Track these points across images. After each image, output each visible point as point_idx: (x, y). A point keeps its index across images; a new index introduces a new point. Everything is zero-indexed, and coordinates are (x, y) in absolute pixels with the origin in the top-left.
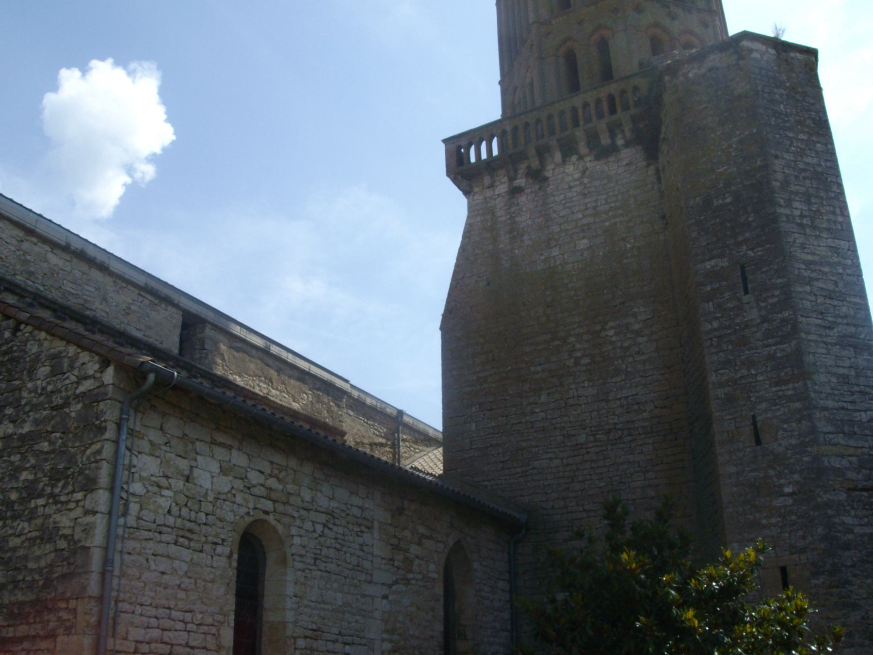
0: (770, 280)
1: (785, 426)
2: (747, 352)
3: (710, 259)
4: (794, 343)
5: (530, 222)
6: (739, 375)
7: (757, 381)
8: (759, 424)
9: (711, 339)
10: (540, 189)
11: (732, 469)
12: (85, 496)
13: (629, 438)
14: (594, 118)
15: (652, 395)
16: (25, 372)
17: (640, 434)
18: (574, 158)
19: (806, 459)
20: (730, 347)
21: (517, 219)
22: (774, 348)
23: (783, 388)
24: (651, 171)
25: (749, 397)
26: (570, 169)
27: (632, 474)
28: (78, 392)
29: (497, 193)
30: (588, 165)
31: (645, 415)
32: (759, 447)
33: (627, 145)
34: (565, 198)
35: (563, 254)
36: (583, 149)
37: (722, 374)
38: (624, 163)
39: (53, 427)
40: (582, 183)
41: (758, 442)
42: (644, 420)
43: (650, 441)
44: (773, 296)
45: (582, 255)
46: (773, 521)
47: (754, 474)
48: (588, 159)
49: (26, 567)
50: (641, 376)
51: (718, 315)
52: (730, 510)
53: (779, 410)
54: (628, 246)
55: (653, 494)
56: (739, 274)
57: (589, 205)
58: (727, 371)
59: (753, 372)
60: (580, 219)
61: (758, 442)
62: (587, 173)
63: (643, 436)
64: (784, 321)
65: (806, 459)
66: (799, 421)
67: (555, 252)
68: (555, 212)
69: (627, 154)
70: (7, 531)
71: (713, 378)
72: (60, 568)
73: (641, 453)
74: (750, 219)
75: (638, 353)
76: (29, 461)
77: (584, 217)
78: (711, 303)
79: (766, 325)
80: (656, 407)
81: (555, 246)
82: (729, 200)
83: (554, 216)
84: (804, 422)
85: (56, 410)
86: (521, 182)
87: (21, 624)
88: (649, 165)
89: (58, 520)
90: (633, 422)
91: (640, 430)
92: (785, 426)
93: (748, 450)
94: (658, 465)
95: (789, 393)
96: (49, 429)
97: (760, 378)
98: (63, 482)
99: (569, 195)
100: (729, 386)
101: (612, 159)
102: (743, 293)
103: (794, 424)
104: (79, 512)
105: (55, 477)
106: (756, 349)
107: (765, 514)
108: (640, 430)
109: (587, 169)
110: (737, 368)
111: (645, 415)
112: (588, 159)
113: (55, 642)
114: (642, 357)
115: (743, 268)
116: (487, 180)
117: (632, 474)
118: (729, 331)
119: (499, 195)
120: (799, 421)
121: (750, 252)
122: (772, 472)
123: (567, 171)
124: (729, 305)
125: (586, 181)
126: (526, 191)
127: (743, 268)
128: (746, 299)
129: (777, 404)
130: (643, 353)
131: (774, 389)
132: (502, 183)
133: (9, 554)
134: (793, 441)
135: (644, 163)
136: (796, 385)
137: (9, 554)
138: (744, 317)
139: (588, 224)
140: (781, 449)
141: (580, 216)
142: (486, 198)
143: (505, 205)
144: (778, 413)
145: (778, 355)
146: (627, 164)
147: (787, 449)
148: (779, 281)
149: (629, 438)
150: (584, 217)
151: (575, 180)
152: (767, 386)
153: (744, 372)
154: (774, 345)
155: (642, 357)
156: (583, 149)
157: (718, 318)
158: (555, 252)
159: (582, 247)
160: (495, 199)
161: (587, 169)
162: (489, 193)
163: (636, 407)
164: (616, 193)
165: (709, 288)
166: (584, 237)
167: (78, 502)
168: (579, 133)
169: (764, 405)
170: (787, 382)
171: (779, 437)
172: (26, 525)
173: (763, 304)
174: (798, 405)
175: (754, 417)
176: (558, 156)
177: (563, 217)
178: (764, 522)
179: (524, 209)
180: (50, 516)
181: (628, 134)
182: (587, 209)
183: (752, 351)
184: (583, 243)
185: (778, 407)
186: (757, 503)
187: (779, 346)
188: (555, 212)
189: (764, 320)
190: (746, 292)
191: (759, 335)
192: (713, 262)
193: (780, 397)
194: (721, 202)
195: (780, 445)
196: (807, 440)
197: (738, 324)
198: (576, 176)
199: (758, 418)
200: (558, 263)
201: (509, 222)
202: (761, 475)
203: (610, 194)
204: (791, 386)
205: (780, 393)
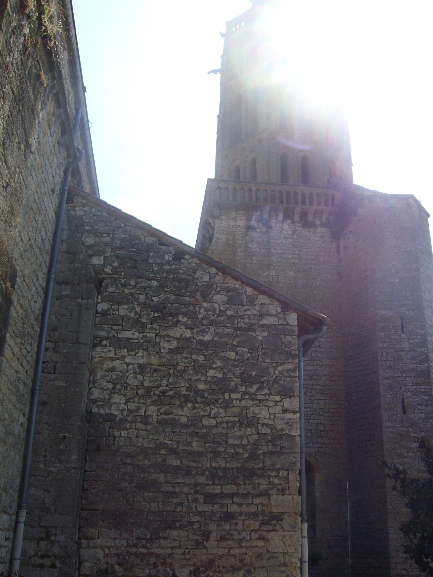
0: (416, 330)
1: (419, 407)
2: (401, 364)
3: (385, 309)
4: (426, 365)
5: (258, 250)
6: (396, 375)
7: (406, 380)
8: (405, 403)
9: (382, 352)
10: (266, 232)
11: (390, 424)
12: (282, 399)
13: (311, 394)
14: (323, 205)
15: (326, 372)
16: (198, 294)
17: (317, 393)
18: (289, 221)
19: (428, 426)
20: (392, 359)
21: (250, 245)
22: (416, 365)
23: (419, 387)
24: (334, 245)
25: (401, 388)
26: (286, 227)
27: (311, 415)
28: (262, 323)
29: (237, 224)
30: (297, 228)
31: (320, 383)
32: (404, 416)
33: (322, 225)
34: (282, 243)
35: (278, 276)
36: (297, 218)
37: (387, 373)
38: (319, 235)
39: (238, 342)
40: (292, 238)
41: (404, 412)
42: (320, 385)
43: (323, 398)
44: (417, 338)
45: (290, 280)
46: (410, 455)
47: (401, 429)
48: (297, 225)
49: (227, 442)
50: (320, 360)
51: (387, 340)
52: (388, 445)
53: (416, 398)
54: (318, 284)
55: (322, 428)
56: (400, 322)
57: (296, 252)
58: (390, 371)
59: (404, 375)
60: (290, 259)
61: (404, 412)
62: (296, 233)
63: (319, 395)
64: (422, 352)
65: (428, 426)
66: (426, 406)
67: (273, 273)
68: (275, 249)
69: (321, 230)
70: (199, 412)
71: (382, 373)
72: (265, 447)
73: (317, 404)
74: (408, 295)
75: (319, 346)
76: (216, 363)
77: (292, 258)
78: (383, 333)
79: (412, 352)
80: (327, 380)
81: (273, 270)
82: (397, 281)
83: (273, 251)
84: (429, 407)
85: (240, 331)
86: (254, 223)
87: (228, 484)
88: (332, 241)
89: (256, 412)
90: (313, 385)
91: (318, 391)
92: (419, 407)
93: (399, 415)
94: (326, 412)
95: (423, 390)
96: (234, 343)
97: (408, 379)
98: (258, 385)
99: (284, 242)
100: (391, 380)
101: (312, 230)
102: (401, 332)
103: (423, 407)
104: (278, 409)
105: (246, 379)
106: (407, 364)
107: (406, 451)
108: (318, 391)
109: (296, 230)
110: (396, 371)
111: (320, 383)
112: (297, 225)
113: (270, 500)
114: (321, 350)
115: (402, 319)
116: (233, 214)
117: (311, 415)
118: (392, 351)
119: (239, 226)
120: (426, 406)
121: (406, 312)
122: (411, 430)
123: (284, 227)
124: (393, 337)
125: (295, 237)
126: (257, 230)
127: (402, 319)
128: (403, 336)
129: (416, 395)
130: (322, 347)
131: (415, 387)
132: (241, 220)
133: (204, 431)
134: (423, 416)
135: (330, 239)
136: (426, 387)
137: (204, 431)
138: (401, 345)
139: (294, 263)
140: (416, 418)
141: (290, 257)
142: (229, 225)
143: (242, 234)
144: (416, 400)
145: (418, 370)
146: (321, 237)
147: (419, 419)
148: (421, 331)
149: (311, 394)
150: (292, 258)
151: (288, 235)
152: (411, 384)
153: (399, 374)
154: (416, 364)
155: (321, 350)
156: (297, 218)
157: (387, 342)
158: (273, 273)
159: (290, 275)
160: (236, 228)
161: (296, 230)
162: (232, 223)
163: (316, 377)
164: (313, 251)
165: (383, 325)
166: (291, 270)
167: (276, 402)
168: (298, 209)
169: (408, 394)
170: (422, 385)
171: (416, 412)
172: (221, 410)
173: (411, 341)
174: (426, 397)
175: (403, 399)
176: (281, 217)
177: (280, 254)
178: (405, 454)
179: (255, 241)
180: (248, 408)
181: (324, 219)
182: (295, 254)
183: (404, 364)
184: (291, 274)
185: (416, 396)
186: (402, 444)
187: (418, 365)
188: (275, 249)
189: (411, 350)
190: (403, 333)
191: (408, 357)
192: (386, 312)
193: (417, 391)
194: (392, 280)
195: (416, 416)
196: (430, 416)
197: (397, 348)
198: (289, 232)
199: (405, 400)
200: (274, 280)
201: (244, 245)
202: (405, 430)
203: (309, 250)
204: (423, 387)
205: (418, 389)
